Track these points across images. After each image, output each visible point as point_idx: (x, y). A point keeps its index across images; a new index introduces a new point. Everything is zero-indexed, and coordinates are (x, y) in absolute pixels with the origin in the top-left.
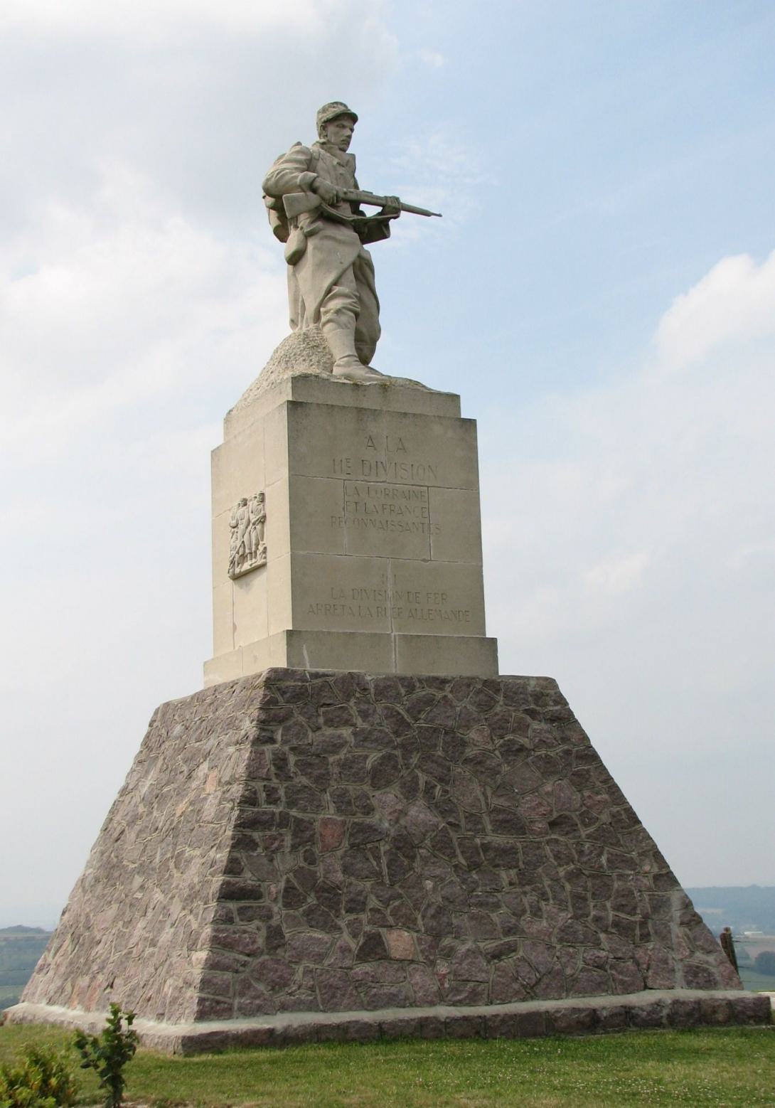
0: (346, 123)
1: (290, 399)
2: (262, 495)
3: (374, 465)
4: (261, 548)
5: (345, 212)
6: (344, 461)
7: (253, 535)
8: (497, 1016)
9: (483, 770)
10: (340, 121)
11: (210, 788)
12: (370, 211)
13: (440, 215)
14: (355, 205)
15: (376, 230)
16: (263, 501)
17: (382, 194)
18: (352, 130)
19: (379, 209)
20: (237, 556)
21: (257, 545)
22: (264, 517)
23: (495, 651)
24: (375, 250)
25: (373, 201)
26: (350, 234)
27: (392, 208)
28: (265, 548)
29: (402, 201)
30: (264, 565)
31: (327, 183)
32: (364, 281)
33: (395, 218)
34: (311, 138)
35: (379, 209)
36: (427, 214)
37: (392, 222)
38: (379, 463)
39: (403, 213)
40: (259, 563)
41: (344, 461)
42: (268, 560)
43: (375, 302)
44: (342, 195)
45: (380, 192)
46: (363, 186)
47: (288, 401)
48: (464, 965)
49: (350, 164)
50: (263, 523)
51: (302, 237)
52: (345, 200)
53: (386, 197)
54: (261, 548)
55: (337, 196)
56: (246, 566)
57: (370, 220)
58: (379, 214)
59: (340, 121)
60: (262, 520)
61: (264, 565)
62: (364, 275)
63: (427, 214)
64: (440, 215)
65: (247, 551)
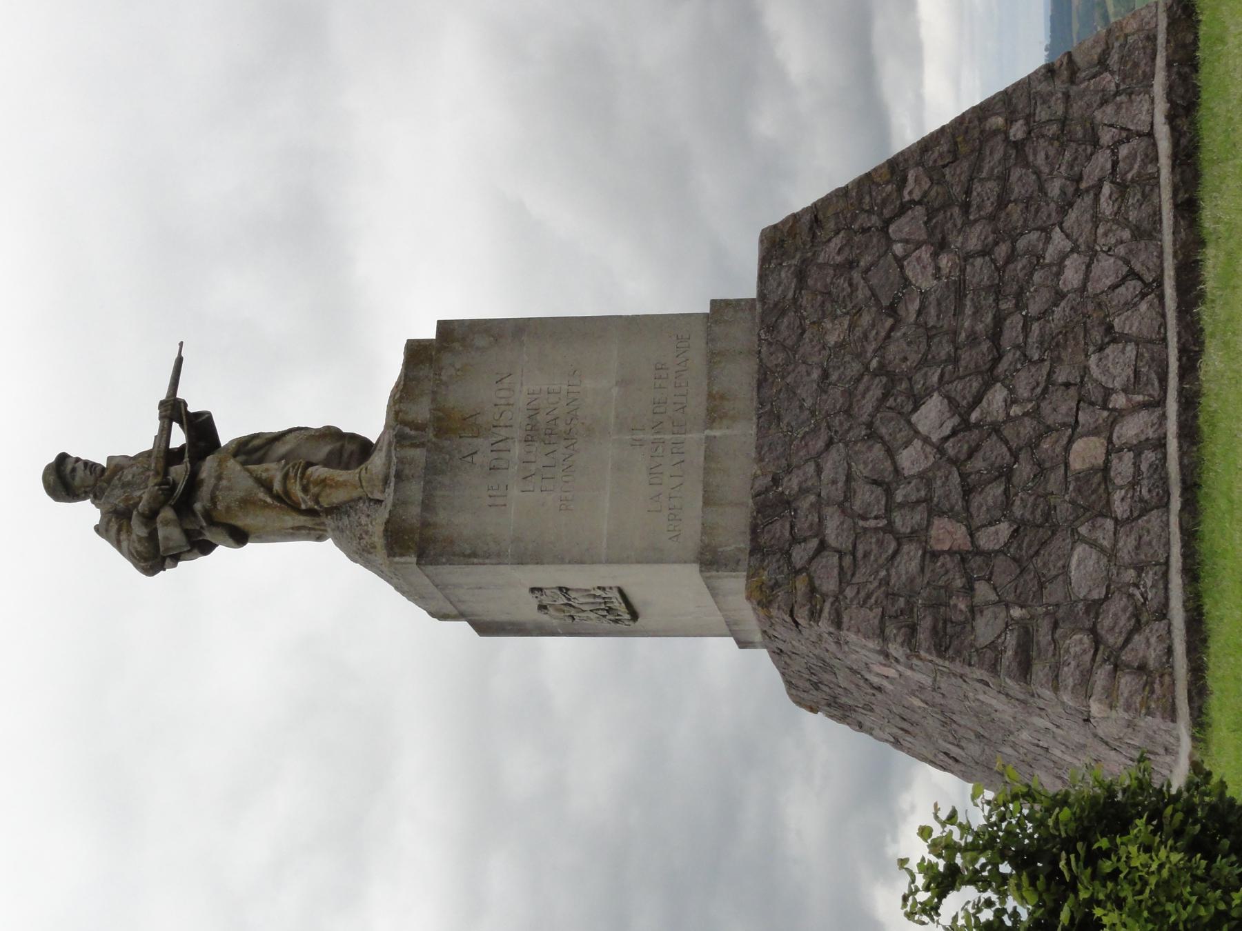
0: (69, 467)
1: (414, 559)
2: (533, 590)
3: (495, 455)
4: (599, 593)
5: (179, 472)
6: (490, 492)
7: (582, 600)
8: (1179, 334)
9: (874, 332)
10: (65, 479)
11: (892, 672)
12: (178, 437)
13: (181, 344)
14: (172, 457)
15: (201, 427)
16: (540, 589)
17: (157, 423)
18: (78, 460)
19: (175, 426)
20: (609, 617)
21: (595, 596)
22: (560, 589)
23: (727, 303)
24: (227, 434)
25: (165, 433)
26: (209, 467)
27: (173, 409)
28: (599, 588)
29: (164, 397)
30: (621, 591)
31: (145, 496)
32: (262, 452)
33: (186, 405)
34: (87, 512)
35: (175, 426)
36: (179, 361)
37: (191, 409)
38: (495, 447)
39: (180, 395)
40: (618, 595)
41: (490, 492)
42: (613, 584)
43: (293, 434)
44: (159, 479)
45: (154, 426)
46: (149, 445)
47: (418, 563)
48: (1115, 372)
49: (118, 465)
50: (567, 589)
51: (214, 529)
52: (166, 473)
53: (161, 418)
54: (599, 593)
55: (160, 484)
56: (622, 608)
57: (189, 437)
58: (182, 426)
59: (65, 479)
60: (564, 590)
61: (621, 591)
62: (257, 449)
63: (179, 361)
64: (181, 344)
65: (603, 606)
